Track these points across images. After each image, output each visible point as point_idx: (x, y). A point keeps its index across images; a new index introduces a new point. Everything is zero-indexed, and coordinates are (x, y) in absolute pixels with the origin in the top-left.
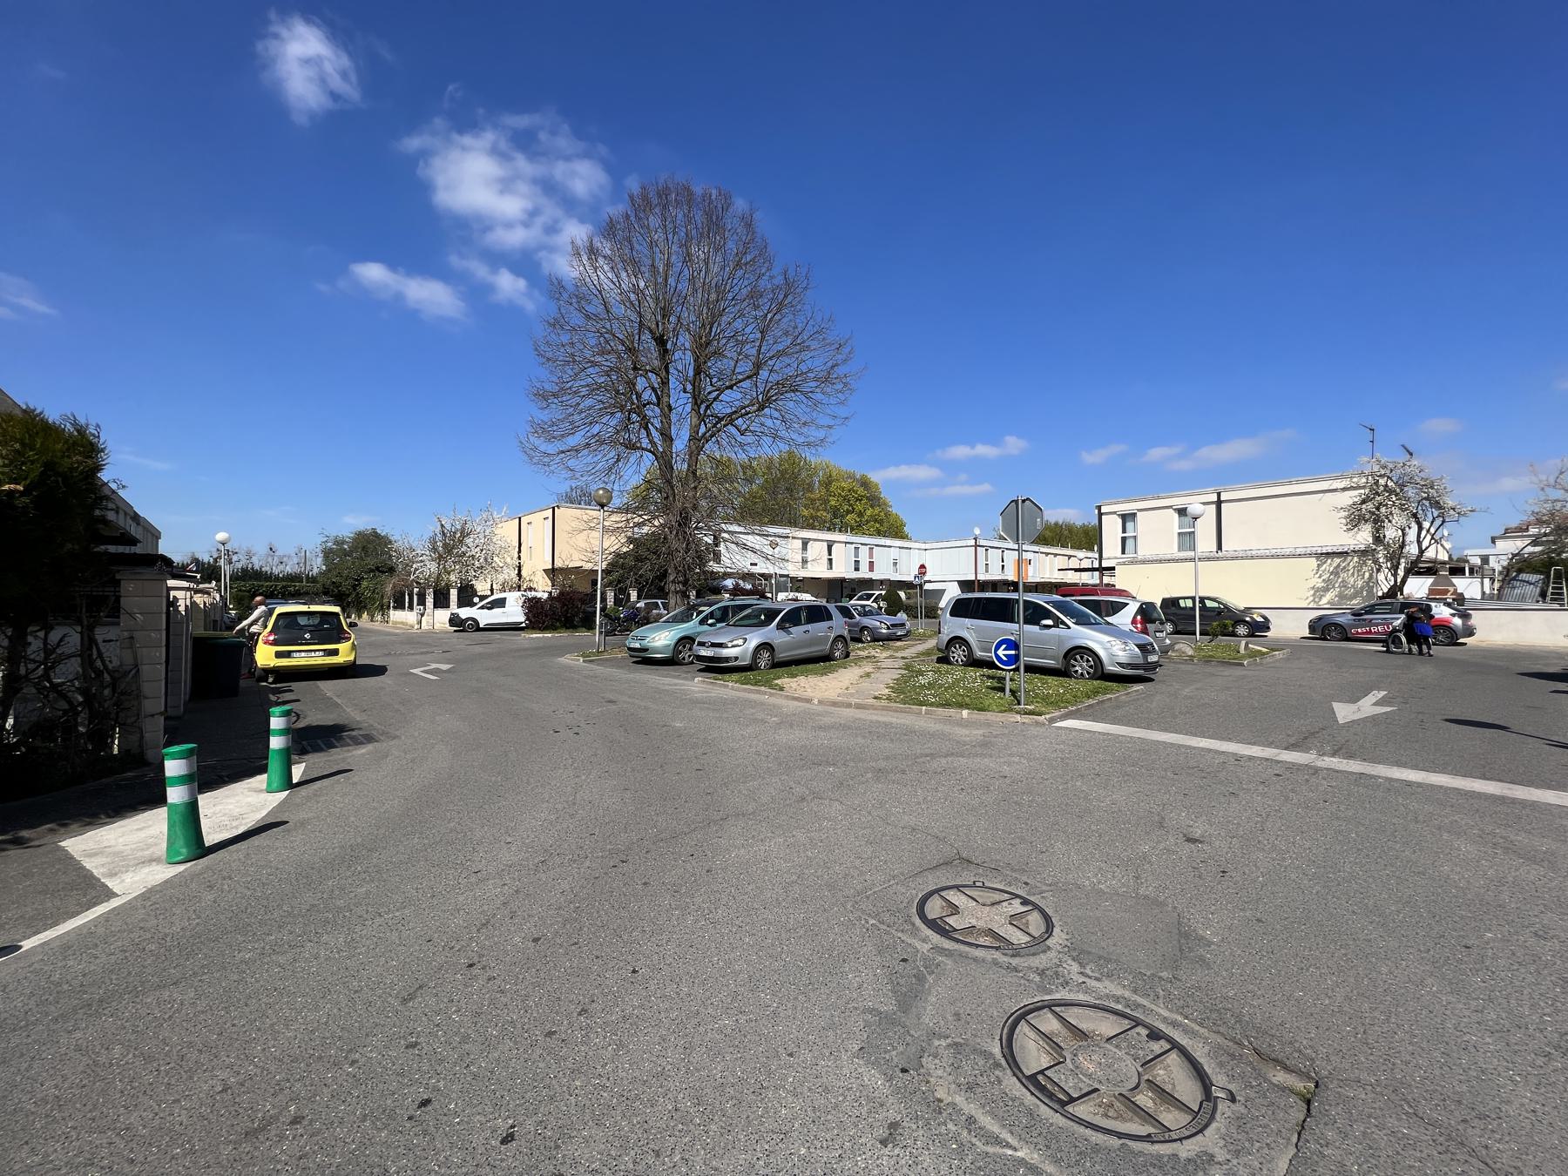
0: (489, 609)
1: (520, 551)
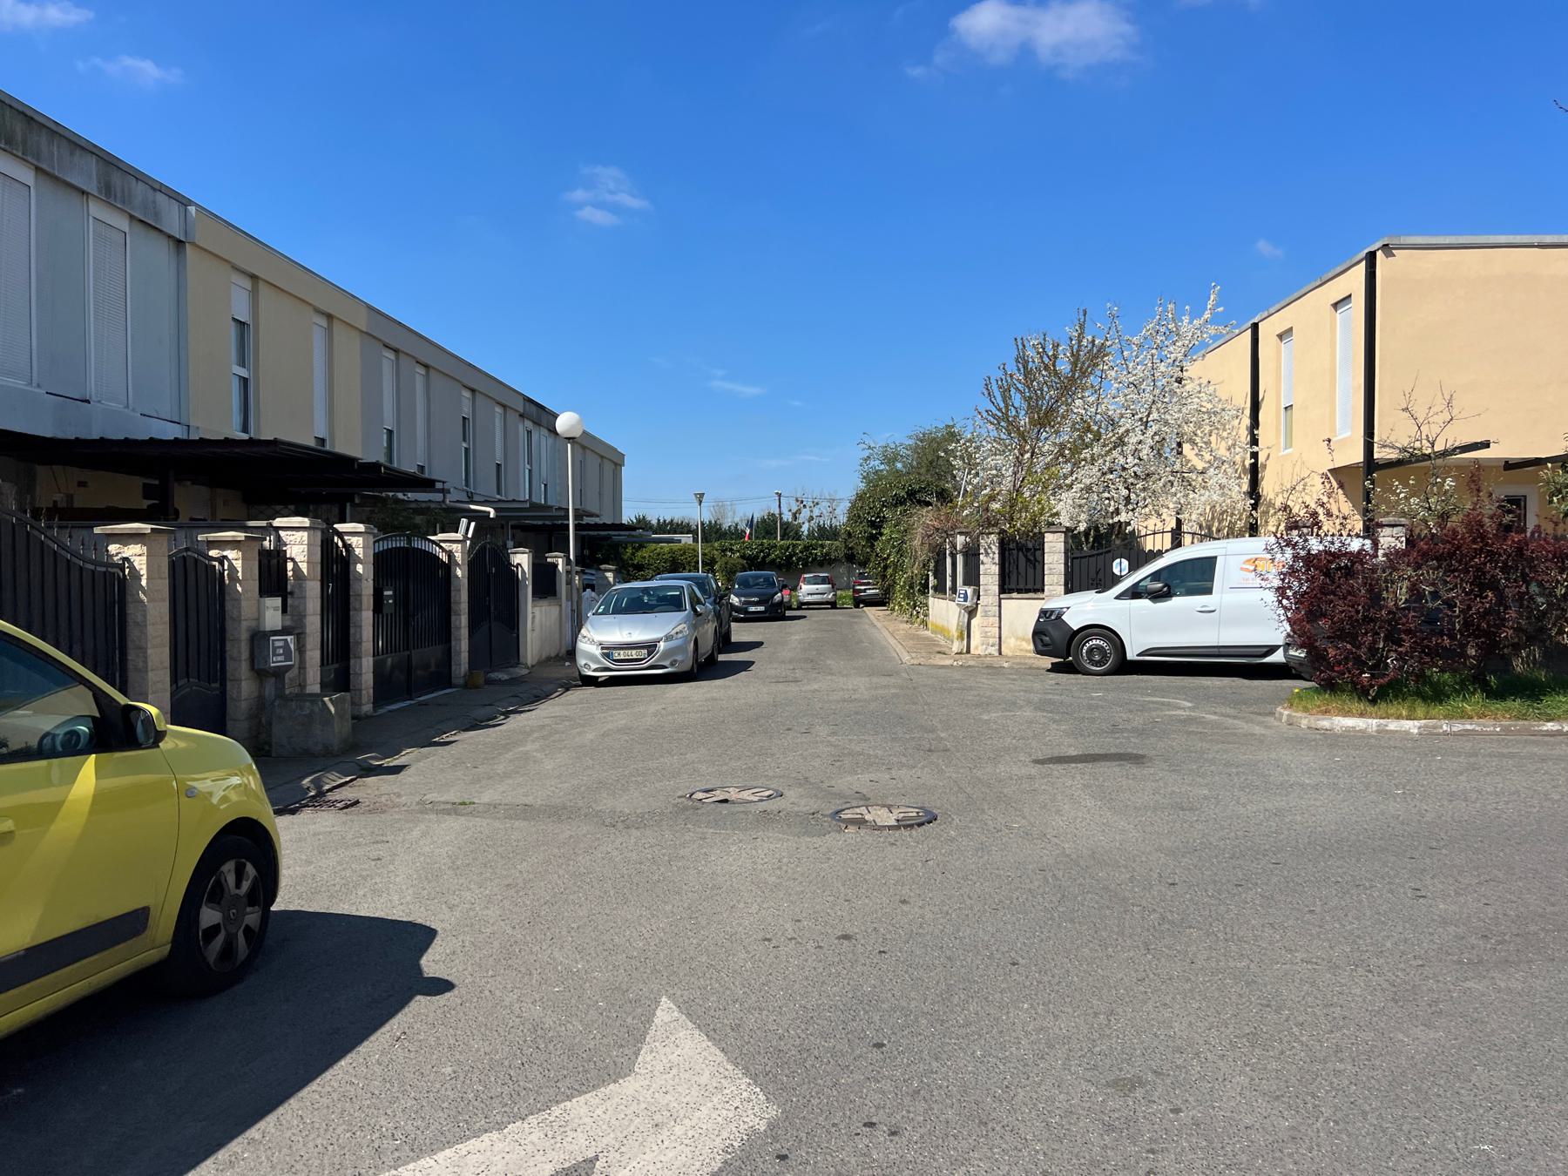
0: (1157, 596)
1: (1255, 423)
